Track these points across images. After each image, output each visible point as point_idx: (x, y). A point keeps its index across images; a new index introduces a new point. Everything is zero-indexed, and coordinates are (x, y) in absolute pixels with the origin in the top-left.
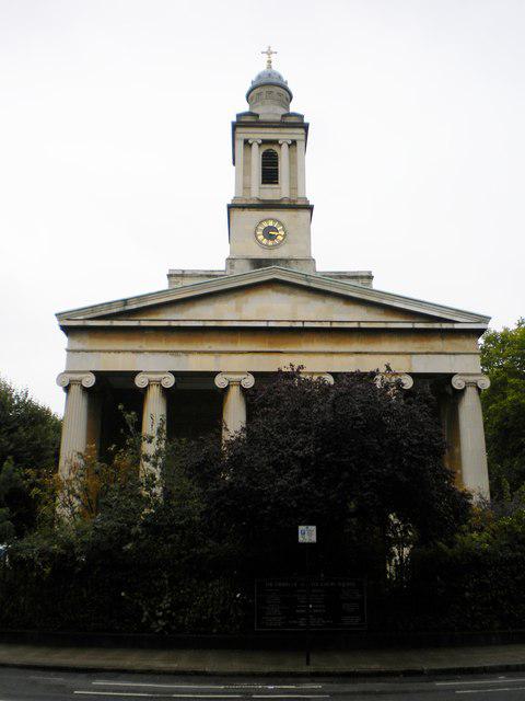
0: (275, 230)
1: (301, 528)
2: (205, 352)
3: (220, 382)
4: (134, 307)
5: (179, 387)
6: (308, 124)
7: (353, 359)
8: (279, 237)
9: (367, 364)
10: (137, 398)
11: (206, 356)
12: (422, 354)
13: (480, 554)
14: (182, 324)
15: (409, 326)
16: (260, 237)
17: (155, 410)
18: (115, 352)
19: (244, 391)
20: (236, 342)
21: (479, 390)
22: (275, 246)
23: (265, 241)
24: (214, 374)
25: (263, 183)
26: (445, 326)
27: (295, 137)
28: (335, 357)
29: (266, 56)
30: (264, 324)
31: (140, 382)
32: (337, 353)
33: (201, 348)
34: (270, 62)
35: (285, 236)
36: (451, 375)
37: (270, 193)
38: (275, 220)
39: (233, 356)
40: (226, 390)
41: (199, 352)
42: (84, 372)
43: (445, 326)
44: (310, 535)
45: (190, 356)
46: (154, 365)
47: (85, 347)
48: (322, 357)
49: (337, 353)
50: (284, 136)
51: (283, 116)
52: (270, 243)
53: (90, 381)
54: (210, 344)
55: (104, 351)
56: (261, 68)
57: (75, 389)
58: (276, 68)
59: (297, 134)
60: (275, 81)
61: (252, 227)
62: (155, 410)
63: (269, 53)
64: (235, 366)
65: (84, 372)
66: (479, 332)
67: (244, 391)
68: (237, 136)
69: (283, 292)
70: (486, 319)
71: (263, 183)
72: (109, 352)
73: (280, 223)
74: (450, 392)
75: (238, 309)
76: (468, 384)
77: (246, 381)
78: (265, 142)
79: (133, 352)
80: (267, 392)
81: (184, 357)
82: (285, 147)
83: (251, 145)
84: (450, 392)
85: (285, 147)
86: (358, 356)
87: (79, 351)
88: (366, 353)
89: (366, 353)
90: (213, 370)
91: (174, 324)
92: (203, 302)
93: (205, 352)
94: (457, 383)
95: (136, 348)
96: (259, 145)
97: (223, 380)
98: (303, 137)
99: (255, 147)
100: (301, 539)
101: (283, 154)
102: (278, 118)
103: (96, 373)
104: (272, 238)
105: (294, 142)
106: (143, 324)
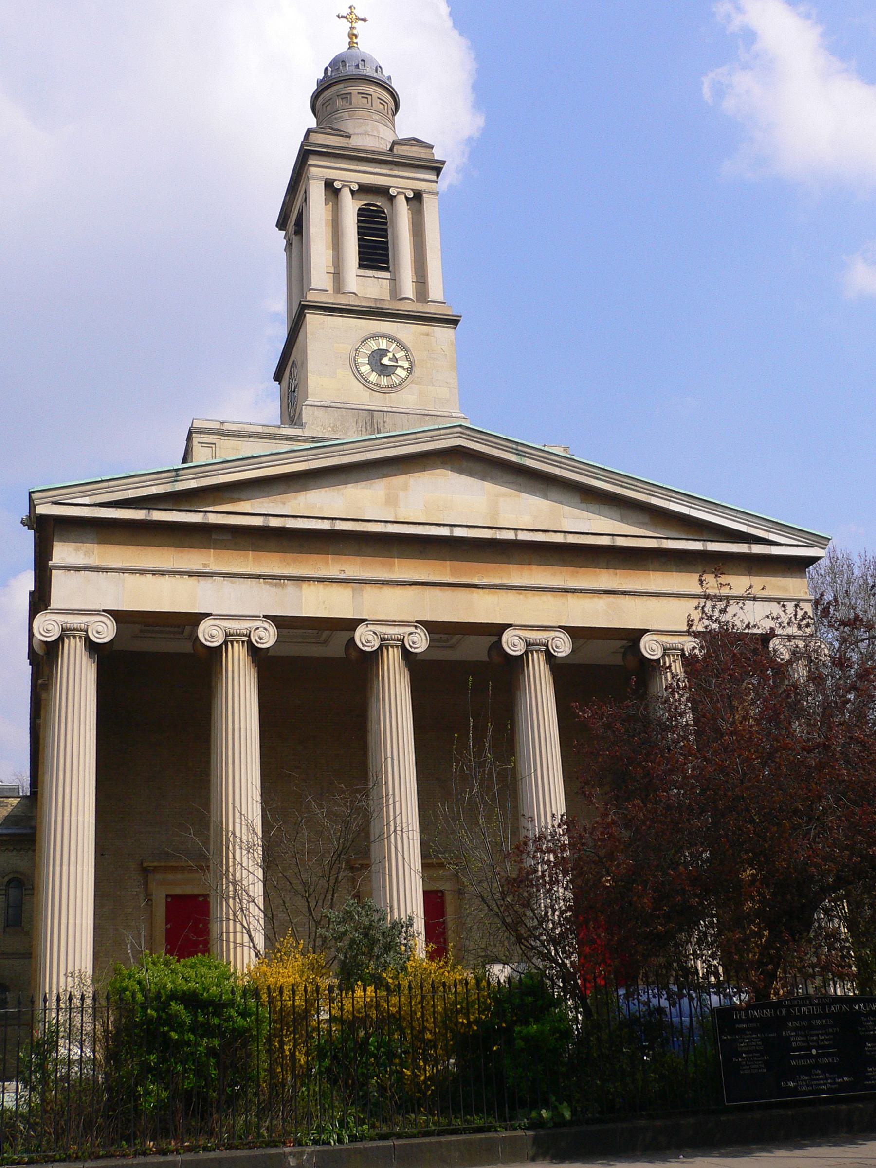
0: (383, 353)
2: (333, 580)
4: (193, 484)
7: (602, 602)
8: (399, 371)
9: (481, 608)
12: (181, 573)
14: (291, 523)
15: (697, 546)
16: (365, 369)
18: (154, 572)
20: (392, 565)
22: (393, 388)
23: (373, 377)
24: (353, 624)
26: (757, 549)
28: (571, 598)
29: (345, 25)
30: (444, 532)
32: (575, 591)
33: (323, 573)
34: (352, 35)
35: (410, 370)
38: (391, 339)
41: (321, 580)
42: (254, 618)
45: (305, 585)
46: (233, 602)
47: (94, 561)
48: (548, 597)
49: (575, 591)
50: (400, 183)
52: (384, 381)
55: (133, 571)
56: (341, 46)
58: (365, 46)
59: (420, 181)
60: (369, 71)
61: (347, 348)
63: (351, 17)
65: (254, 618)
66: (797, 565)
67: (92, 647)
69: (471, 474)
70: (821, 541)
72: (143, 572)
73: (402, 346)
75: (391, 501)
77: (415, 638)
78: (364, 189)
79: (191, 574)
82: (401, 202)
86: (611, 598)
87: (77, 569)
88: (624, 593)
89: (624, 593)
91: (274, 522)
92: (605, 509)
93: (333, 580)
94: (650, 647)
95: (197, 567)
96: (353, 192)
99: (346, 194)
104: (385, 370)
106: (213, 519)
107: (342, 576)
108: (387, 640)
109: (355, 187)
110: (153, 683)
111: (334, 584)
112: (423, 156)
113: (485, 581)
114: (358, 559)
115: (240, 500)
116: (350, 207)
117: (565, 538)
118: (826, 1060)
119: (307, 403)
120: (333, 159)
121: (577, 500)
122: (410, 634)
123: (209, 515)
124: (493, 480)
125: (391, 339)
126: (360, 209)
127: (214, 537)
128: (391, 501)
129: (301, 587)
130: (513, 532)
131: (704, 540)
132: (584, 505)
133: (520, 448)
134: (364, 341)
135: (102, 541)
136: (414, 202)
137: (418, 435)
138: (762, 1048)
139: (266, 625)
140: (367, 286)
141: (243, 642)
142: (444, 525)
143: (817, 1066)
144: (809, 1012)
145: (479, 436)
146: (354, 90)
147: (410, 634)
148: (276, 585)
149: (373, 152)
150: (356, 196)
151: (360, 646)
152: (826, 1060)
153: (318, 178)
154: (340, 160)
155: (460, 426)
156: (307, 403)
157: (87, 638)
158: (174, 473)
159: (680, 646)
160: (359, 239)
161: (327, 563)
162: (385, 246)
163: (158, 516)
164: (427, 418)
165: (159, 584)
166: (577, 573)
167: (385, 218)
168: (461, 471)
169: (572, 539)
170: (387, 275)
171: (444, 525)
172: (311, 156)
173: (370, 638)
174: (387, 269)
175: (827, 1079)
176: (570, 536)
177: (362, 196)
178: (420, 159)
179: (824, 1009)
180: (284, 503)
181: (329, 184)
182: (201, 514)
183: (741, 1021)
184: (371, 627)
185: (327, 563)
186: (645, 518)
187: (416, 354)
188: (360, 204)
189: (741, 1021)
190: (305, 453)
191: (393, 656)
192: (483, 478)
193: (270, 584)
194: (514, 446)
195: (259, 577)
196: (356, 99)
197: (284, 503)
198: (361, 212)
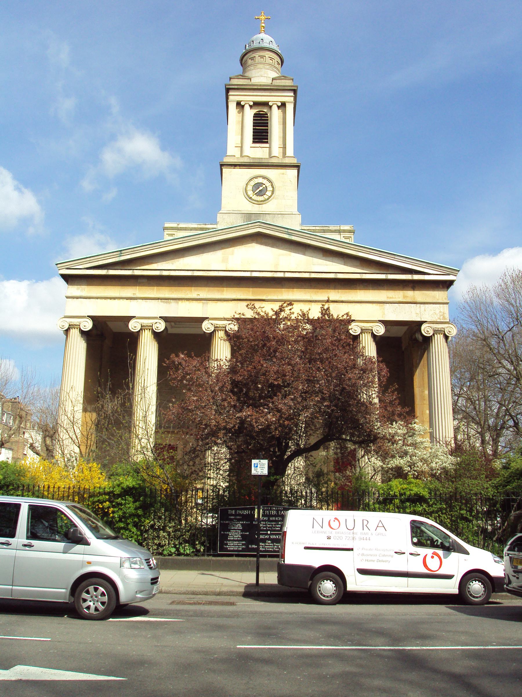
0: (261, 184)
1: (254, 462)
3: (207, 327)
5: (170, 331)
6: (15, 190)
10: (132, 340)
11: (195, 302)
13: (363, 479)
17: (148, 355)
19: (157, 335)
20: (223, 291)
21: (446, 337)
24: (202, 320)
25: (254, 142)
26: (416, 277)
27: (283, 99)
31: (133, 326)
35: (273, 192)
36: (421, 323)
37: (259, 152)
38: (264, 178)
39: (219, 303)
40: (211, 335)
43: (416, 277)
44: (262, 468)
45: (180, 302)
46: (145, 310)
51: (273, 79)
53: (88, 325)
54: (197, 293)
57: (75, 333)
62: (148, 355)
64: (219, 312)
68: (231, 98)
71: (254, 142)
74: (420, 338)
75: (225, 260)
76: (436, 332)
78: (256, 104)
79: (127, 299)
80: (254, 339)
81: (173, 303)
82: (275, 108)
83: (243, 107)
84: (420, 338)
85: (275, 108)
88: (342, 302)
89: (342, 302)
90: (423, 320)
92: (242, 244)
94: (426, 330)
96: (251, 107)
97: (210, 326)
98: (292, 99)
99: (247, 107)
100: (254, 472)
101: (275, 115)
102: (269, 82)
103: (93, 318)
104: (261, 193)
105: (283, 105)
106: (137, 273)
107: (198, 297)
108: (218, 327)
109: (252, 104)
110: (109, 347)
111: (194, 301)
112: (287, 84)
113: (269, 297)
114: (207, 289)
115: (152, 263)
116: (249, 114)
117: (310, 275)
118: (274, 537)
119: (220, 212)
120: (241, 91)
121: (321, 255)
122: (229, 324)
123: (135, 271)
124: (277, 247)
125: (264, 178)
126: (255, 114)
127: (139, 281)
128: (225, 260)
129: (178, 303)
130: (282, 273)
131: (386, 274)
132: (324, 258)
133: (289, 231)
134: (251, 180)
135: (89, 285)
136: (283, 108)
137: (237, 228)
138: (241, 528)
139: (160, 321)
140: (259, 152)
141: (150, 329)
142: (248, 271)
143: (269, 539)
144: (269, 513)
145: (268, 226)
146: (257, 55)
147: (229, 324)
148: (166, 302)
149: (261, 85)
150: (253, 108)
151: (205, 330)
152: (274, 537)
153: (233, 101)
154: (245, 91)
155: (259, 222)
156: (220, 212)
157: (80, 329)
158: (119, 253)
159: (370, 328)
160: (253, 129)
161: (191, 291)
162: (266, 131)
163: (112, 272)
164: (279, 215)
165: (186, 306)
166: (318, 292)
167: (268, 117)
168: (261, 244)
169: (313, 276)
170: (267, 145)
171: (248, 271)
172: (230, 91)
173: (209, 326)
174: (267, 142)
175: (274, 546)
176: (313, 274)
177: (256, 107)
178: (284, 86)
179: (278, 513)
180: (173, 264)
181: (239, 104)
182: (131, 271)
183: (232, 515)
184: (210, 321)
185: (191, 291)
186: (358, 263)
187: (276, 185)
188: (254, 111)
189: (232, 515)
190: (181, 240)
191: (221, 334)
192: (272, 246)
193: (164, 302)
194: (286, 230)
195: (158, 299)
196: (258, 59)
197: (173, 264)
198: (256, 115)
